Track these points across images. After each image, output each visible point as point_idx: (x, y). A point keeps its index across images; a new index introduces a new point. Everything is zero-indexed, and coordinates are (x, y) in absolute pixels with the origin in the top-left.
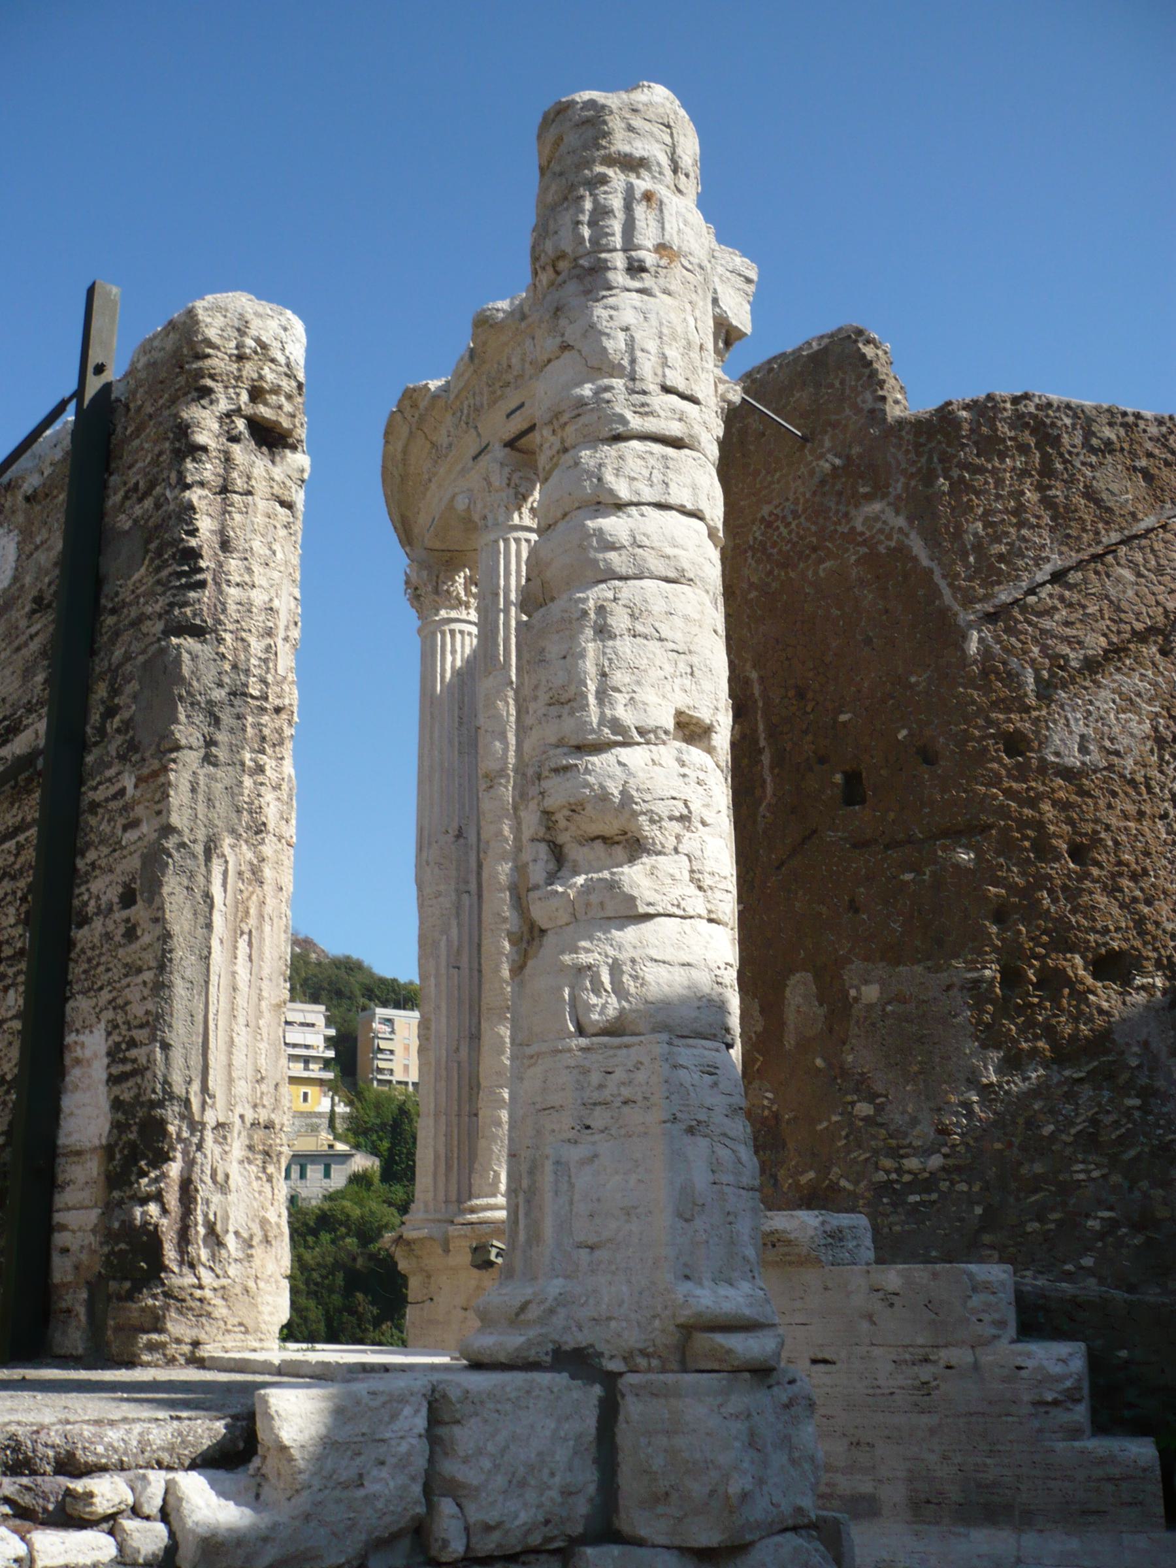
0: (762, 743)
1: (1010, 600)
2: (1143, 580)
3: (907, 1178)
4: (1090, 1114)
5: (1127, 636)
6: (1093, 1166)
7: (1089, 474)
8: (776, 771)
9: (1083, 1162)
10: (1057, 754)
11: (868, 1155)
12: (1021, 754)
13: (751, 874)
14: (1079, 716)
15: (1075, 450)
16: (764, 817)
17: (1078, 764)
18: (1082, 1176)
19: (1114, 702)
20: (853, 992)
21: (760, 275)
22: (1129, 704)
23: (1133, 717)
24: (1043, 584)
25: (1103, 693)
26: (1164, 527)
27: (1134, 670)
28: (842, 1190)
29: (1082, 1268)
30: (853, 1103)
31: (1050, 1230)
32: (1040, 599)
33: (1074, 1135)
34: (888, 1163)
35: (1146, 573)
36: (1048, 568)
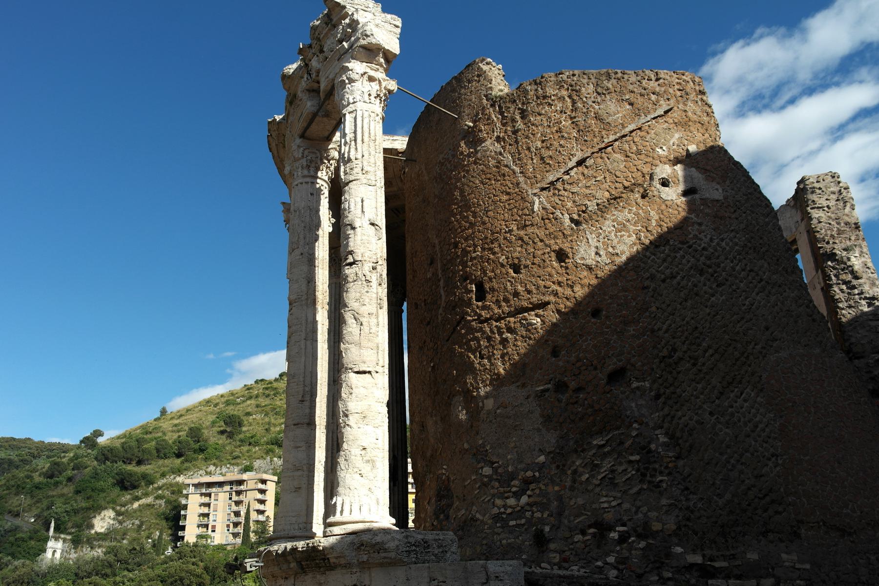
0: (440, 276)
1: (555, 179)
2: (629, 159)
3: (509, 511)
4: (609, 466)
5: (621, 190)
6: (612, 499)
7: (597, 107)
8: (446, 289)
9: (606, 496)
10: (583, 258)
11: (489, 498)
12: (564, 261)
13: (436, 345)
14: (594, 236)
15: (588, 96)
16: (441, 314)
17: (594, 263)
18: (606, 505)
19: (614, 226)
20: (481, 404)
21: (403, 24)
22: (622, 227)
23: (625, 233)
24: (571, 169)
25: (607, 222)
26: (640, 129)
27: (625, 208)
28: (477, 520)
29: (607, 564)
30: (482, 468)
31: (588, 540)
32: (571, 176)
33: (600, 480)
34: (499, 502)
35: (631, 155)
36: (575, 160)
